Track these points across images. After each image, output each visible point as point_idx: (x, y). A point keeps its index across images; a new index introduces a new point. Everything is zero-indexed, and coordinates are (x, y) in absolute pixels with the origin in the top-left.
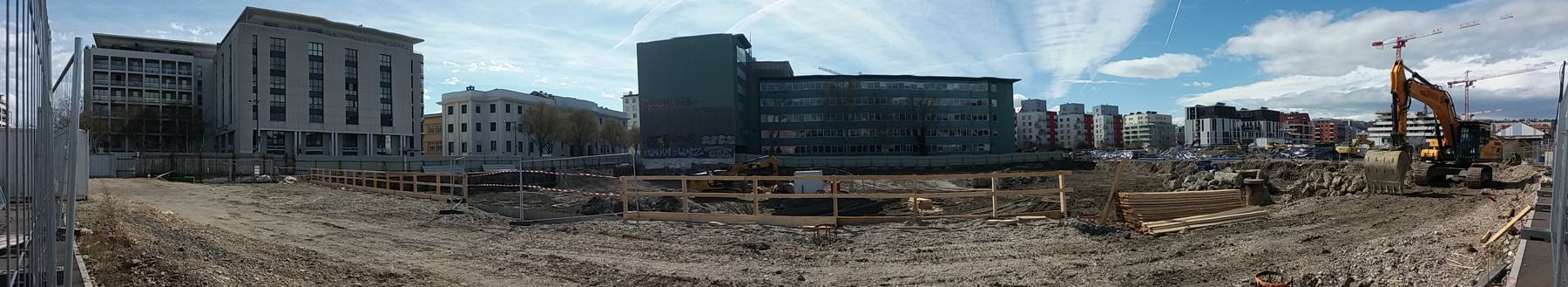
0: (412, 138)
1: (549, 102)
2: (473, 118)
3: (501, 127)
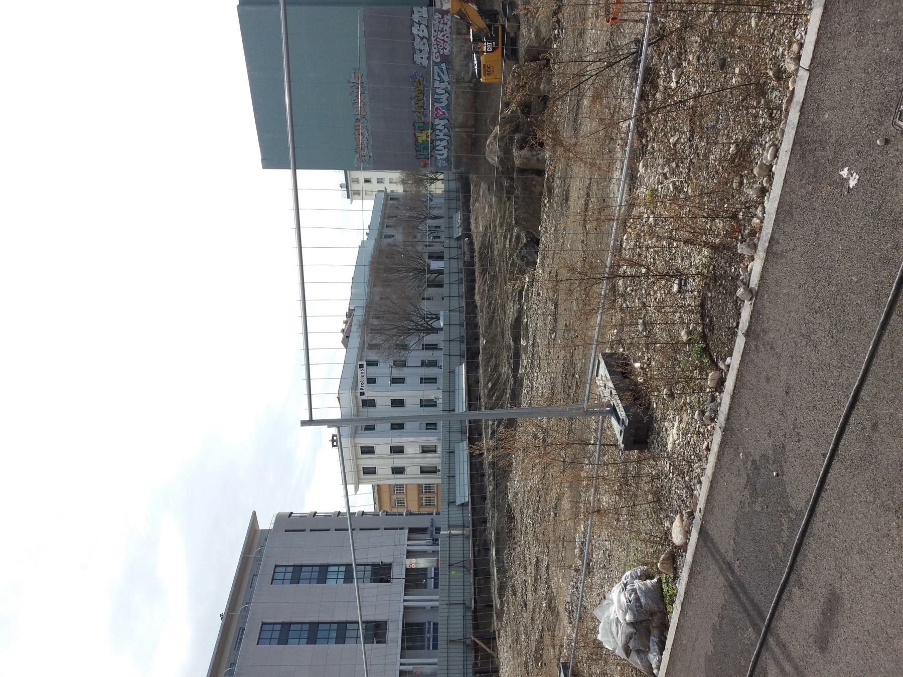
0: (412, 531)
1: (359, 314)
2: (382, 434)
3: (398, 393)
